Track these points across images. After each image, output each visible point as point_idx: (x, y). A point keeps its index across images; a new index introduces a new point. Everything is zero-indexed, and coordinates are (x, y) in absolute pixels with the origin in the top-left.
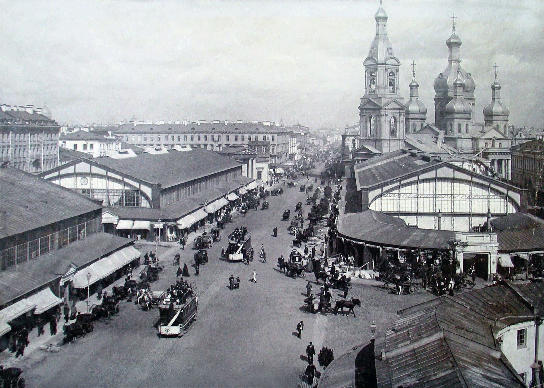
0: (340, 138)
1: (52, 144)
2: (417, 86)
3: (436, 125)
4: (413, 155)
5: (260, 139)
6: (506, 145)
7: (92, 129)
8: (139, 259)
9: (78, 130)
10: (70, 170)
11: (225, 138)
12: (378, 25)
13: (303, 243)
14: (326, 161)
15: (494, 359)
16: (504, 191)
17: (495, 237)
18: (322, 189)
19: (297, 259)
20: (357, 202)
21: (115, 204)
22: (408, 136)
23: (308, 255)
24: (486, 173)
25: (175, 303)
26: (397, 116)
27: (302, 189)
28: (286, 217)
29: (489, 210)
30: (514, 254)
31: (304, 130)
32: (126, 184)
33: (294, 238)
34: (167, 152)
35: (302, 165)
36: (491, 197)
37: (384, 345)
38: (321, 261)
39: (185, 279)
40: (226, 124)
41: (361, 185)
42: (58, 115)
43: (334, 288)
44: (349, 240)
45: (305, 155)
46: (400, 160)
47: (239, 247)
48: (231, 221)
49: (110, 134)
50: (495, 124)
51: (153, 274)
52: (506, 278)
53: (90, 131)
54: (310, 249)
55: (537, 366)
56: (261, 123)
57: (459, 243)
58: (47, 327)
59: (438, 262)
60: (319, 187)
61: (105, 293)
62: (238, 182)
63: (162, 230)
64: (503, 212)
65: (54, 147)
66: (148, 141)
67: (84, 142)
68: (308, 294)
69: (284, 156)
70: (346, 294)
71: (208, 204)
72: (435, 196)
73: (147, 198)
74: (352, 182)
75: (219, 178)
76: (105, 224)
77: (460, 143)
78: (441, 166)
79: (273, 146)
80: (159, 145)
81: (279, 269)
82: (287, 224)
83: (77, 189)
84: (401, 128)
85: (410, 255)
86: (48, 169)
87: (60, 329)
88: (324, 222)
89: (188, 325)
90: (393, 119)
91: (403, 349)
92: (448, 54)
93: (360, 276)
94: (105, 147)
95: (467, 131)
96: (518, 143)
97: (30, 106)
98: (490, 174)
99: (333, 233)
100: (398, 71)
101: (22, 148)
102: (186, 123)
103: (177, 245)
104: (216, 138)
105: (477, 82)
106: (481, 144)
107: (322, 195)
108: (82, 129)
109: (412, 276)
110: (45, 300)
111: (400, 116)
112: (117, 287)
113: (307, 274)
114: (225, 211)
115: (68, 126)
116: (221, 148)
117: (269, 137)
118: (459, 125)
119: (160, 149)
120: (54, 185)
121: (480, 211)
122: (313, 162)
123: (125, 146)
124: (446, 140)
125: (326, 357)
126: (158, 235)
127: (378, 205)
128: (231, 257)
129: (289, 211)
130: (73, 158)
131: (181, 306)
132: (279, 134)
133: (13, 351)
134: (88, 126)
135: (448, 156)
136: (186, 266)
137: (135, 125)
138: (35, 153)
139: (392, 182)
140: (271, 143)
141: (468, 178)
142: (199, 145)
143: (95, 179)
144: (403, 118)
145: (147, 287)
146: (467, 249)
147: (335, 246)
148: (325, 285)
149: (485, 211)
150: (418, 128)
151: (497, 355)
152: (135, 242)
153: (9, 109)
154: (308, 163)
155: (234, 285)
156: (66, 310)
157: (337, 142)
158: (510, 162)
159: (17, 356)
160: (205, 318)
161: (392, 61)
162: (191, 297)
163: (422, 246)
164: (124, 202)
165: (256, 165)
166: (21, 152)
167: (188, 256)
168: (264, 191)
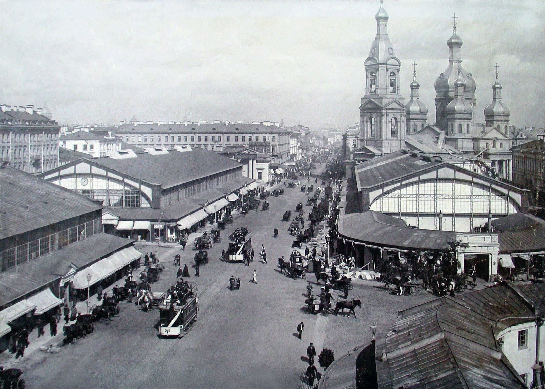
0: (341, 139)
1: (52, 145)
2: (418, 86)
3: (436, 125)
4: (414, 156)
5: (261, 139)
6: (507, 145)
7: (92, 129)
8: (139, 259)
9: (79, 130)
10: (71, 170)
11: (226, 138)
12: (379, 25)
13: (303, 244)
14: (327, 162)
15: (495, 360)
16: (505, 191)
17: (495, 237)
18: (322, 190)
19: (298, 260)
20: (357, 203)
21: (115, 204)
22: (409, 137)
23: (309, 255)
24: (487, 174)
25: (175, 304)
26: (398, 117)
27: (303, 190)
28: (286, 217)
29: (490, 211)
30: (515, 255)
31: (304, 130)
32: (126, 184)
33: (295, 239)
34: (168, 153)
35: (303, 166)
36: (492, 197)
37: (384, 346)
38: (322, 262)
39: (185, 279)
40: (227, 125)
41: (362, 186)
42: (58, 116)
43: (334, 289)
44: (350, 241)
45: (306, 156)
46: (400, 160)
47: (240, 247)
48: (231, 222)
49: (110, 135)
50: (496, 124)
51: (153, 275)
52: (507, 279)
53: (90, 132)
54: (311, 250)
55: (538, 367)
56: (261, 123)
57: (460, 244)
58: (47, 328)
59: (438, 262)
60: (320, 188)
61: (106, 294)
62: (238, 182)
63: (162, 230)
64: (504, 212)
65: (54, 147)
66: (149, 142)
67: (84, 143)
68: (309, 295)
69: (284, 156)
70: (346, 295)
71: (208, 205)
72: (435, 196)
73: (147, 199)
74: (352, 182)
75: (220, 178)
76: (105, 225)
77: (460, 143)
78: (441, 167)
79: (274, 146)
80: (159, 145)
81: (280, 269)
82: (288, 224)
83: (77, 190)
84: (402, 128)
85: (411, 255)
86: (48, 169)
87: (60, 330)
88: (325, 223)
89: (188, 326)
90: (393, 119)
91: (404, 350)
92: (449, 55)
93: (360, 277)
94: (105, 147)
95: (468, 131)
96: (519, 143)
97: (31, 106)
98: (490, 175)
99: (334, 234)
100: (398, 71)
101: (22, 149)
102: (186, 124)
103: (178, 246)
104: (216, 138)
105: (478, 82)
106: (482, 145)
107: (322, 195)
108: (82, 129)
109: (412, 277)
110: (45, 301)
111: (401, 116)
112: (117, 287)
113: (307, 275)
114: (225, 211)
115: (68, 126)
116: (222, 148)
117: (269, 137)
118: (460, 126)
119: (160, 150)
120: (54, 185)
121: (481, 212)
122: (314, 162)
123: (125, 146)
124: (447, 140)
125: (327, 358)
126: (159, 236)
127: (379, 205)
128: (232, 257)
129: (290, 211)
130: (73, 158)
131: (181, 307)
132: (279, 134)
133: (13, 352)
134: (88, 126)
135: (449, 156)
136: (186, 267)
137: (135, 125)
138: (35, 153)
139: (393, 183)
140: (272, 143)
141: (469, 178)
142: (199, 146)
143: (95, 180)
144: (403, 119)
145: (148, 288)
146: (467, 250)
147: (335, 246)
148: (326, 286)
149: (486, 212)
150: (419, 129)
151: (498, 356)
152: (135, 243)
153: (9, 109)
154: (309, 163)
155: (234, 285)
156: (67, 311)
157: (338, 142)
158: (511, 163)
159: (17, 357)
160: (205, 319)
161: (393, 62)
162: (192, 297)
163: (423, 246)
164: (124, 203)
165: (257, 165)
166: (21, 153)
167: (189, 257)
168: (265, 191)
